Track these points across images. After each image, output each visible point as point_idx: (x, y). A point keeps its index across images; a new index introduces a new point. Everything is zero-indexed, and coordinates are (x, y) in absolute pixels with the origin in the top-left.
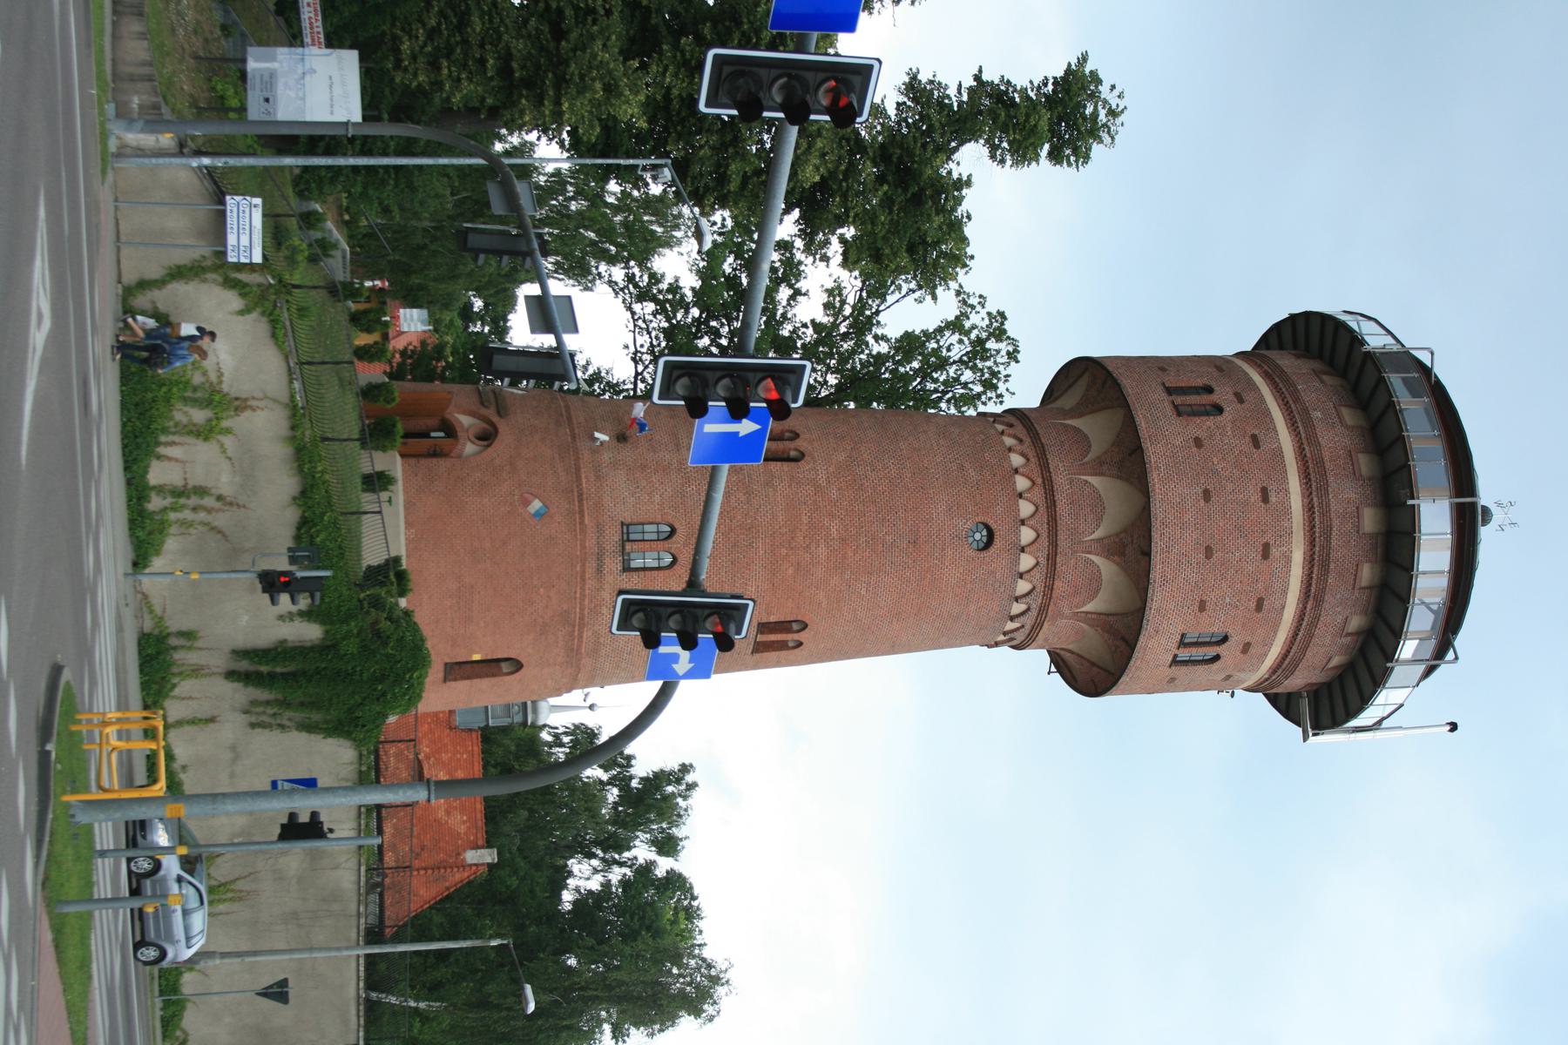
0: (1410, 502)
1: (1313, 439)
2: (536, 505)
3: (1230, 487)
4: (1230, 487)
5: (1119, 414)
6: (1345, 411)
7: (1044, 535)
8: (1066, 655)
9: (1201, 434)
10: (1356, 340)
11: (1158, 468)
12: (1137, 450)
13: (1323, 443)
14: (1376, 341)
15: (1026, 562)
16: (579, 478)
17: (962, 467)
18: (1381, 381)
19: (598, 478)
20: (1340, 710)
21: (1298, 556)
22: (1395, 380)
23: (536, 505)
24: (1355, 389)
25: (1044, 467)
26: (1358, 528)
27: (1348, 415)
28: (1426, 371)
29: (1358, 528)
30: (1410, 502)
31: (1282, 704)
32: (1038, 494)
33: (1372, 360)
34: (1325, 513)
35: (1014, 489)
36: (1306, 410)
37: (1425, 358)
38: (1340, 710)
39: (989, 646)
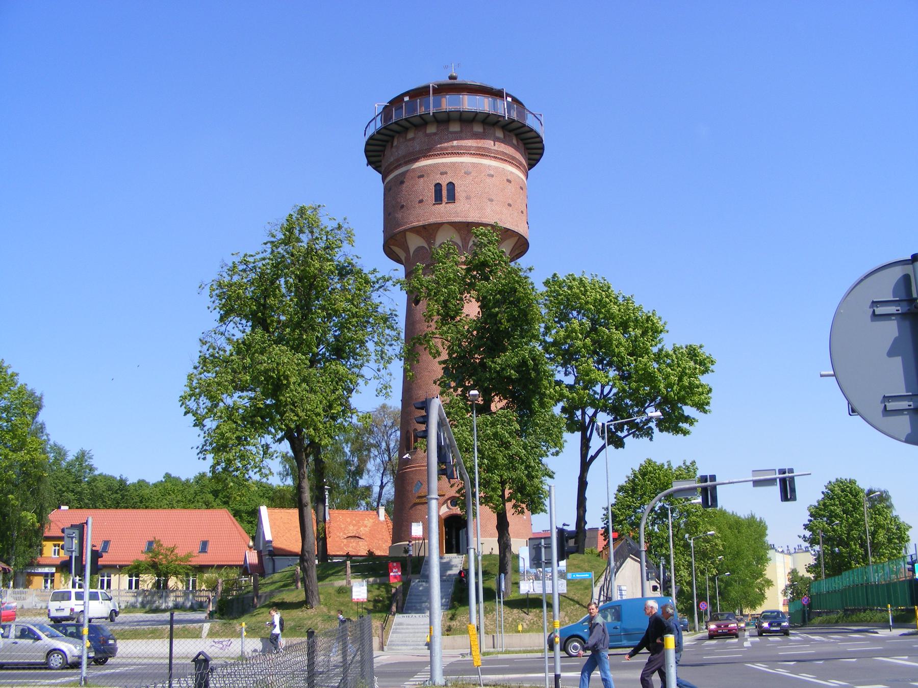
9: (464, 194)
26: (435, 134)
34: (497, 152)
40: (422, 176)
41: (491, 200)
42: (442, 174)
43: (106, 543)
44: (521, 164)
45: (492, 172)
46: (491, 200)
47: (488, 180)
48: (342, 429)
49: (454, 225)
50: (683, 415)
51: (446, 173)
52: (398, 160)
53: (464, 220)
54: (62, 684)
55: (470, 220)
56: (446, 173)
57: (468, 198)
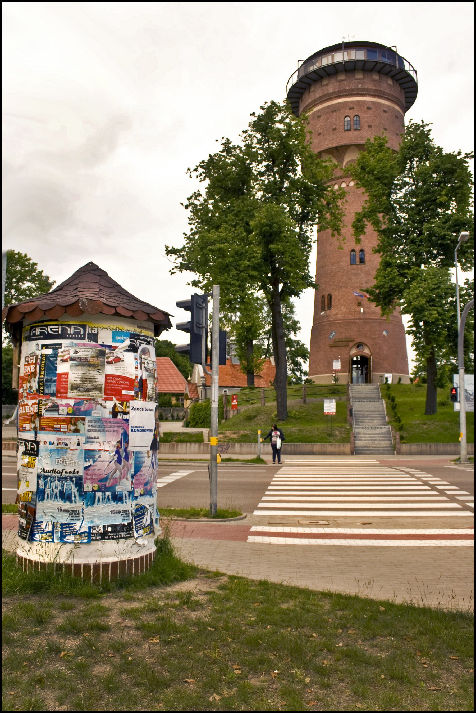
2: (384, 333)
5: (323, 154)
6: (339, 78)
9: (367, 124)
10: (294, 87)
12: (336, 148)
14: (295, 79)
18: (311, 73)
19: (374, 313)
20: (407, 79)
21: (315, 109)
22: (312, 69)
23: (384, 333)
24: (315, 81)
26: (344, 80)
27: (325, 82)
28: (305, 62)
29: (344, 80)
31: (409, 100)
33: (300, 80)
36: (358, 89)
37: (301, 63)
38: (407, 79)
40: (335, 111)
42: (350, 109)
45: (385, 109)
51: (353, 108)
57: (370, 126)
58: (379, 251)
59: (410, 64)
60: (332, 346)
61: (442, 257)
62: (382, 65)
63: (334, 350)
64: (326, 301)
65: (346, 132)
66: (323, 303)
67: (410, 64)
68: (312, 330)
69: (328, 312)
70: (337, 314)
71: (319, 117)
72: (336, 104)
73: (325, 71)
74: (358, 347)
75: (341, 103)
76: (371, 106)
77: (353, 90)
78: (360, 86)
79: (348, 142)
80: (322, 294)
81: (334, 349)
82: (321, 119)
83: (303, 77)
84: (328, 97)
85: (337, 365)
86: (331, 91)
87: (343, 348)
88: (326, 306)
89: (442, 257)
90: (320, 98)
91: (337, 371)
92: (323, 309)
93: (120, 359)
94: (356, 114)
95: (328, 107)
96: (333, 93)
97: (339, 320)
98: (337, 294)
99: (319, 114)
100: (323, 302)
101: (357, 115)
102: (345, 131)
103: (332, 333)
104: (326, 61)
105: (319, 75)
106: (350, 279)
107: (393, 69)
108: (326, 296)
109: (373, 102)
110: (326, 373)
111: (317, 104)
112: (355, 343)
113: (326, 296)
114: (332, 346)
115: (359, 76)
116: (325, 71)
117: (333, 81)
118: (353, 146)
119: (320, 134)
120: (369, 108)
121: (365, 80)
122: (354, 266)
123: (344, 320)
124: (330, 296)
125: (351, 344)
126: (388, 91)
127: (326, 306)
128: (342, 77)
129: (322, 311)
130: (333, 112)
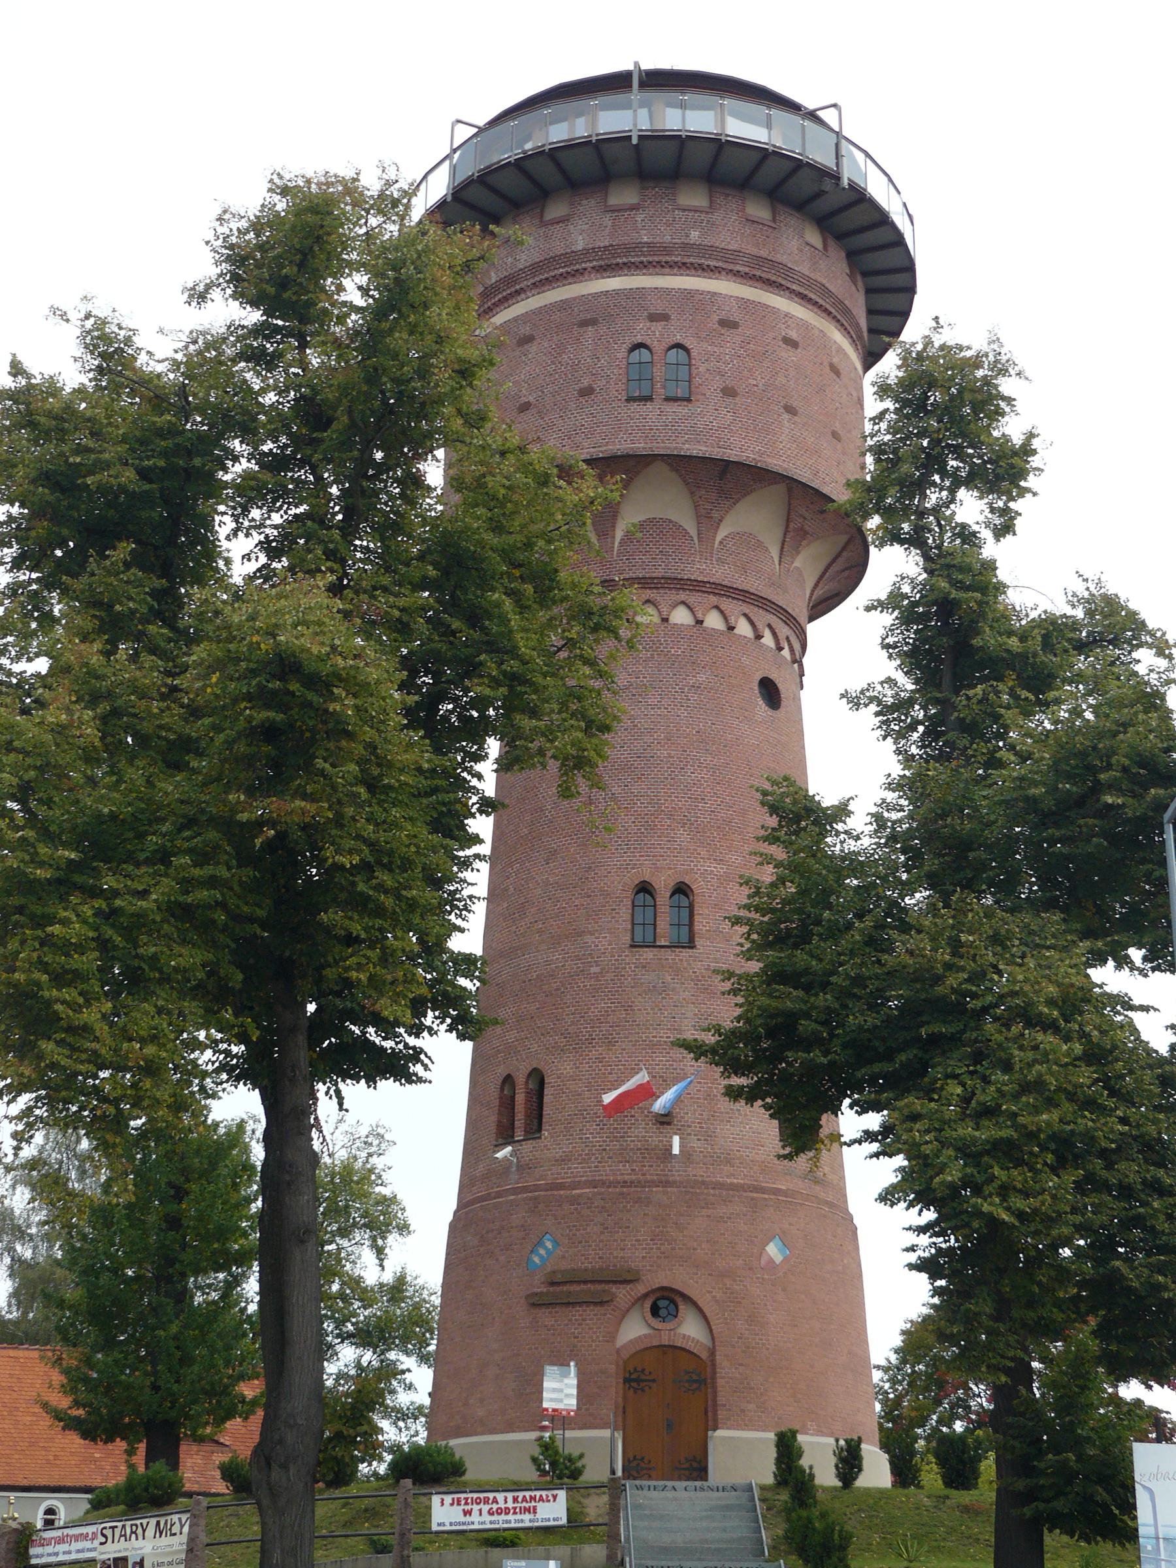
0: (635, 141)
1: (730, 256)
3: (781, 380)
4: (781, 380)
6: (613, 200)
7: (683, 596)
8: (819, 592)
9: (717, 383)
11: (761, 454)
13: (734, 246)
15: (713, 621)
16: (733, 1187)
17: (696, 687)
19: (728, 1162)
25: (697, 586)
26: (634, 208)
27: (556, 209)
29: (634, 208)
30: (635, 141)
31: (884, 322)
32: (665, 598)
34: (808, 282)
35: (722, 633)
36: (686, 246)
39: (802, 674)
40: (593, 322)
41: (791, 410)
42: (653, 318)
43: (1167, 1027)
44: (860, 337)
45: (793, 335)
46: (791, 410)
47: (786, 353)
48: (459, 900)
49: (681, 464)
50: (393, 1287)
51: (665, 317)
52: (509, 280)
53: (717, 453)
54: (430, 1058)
55: (733, 455)
56: (665, 317)
57: (729, 392)
58: (774, 809)
59: (890, 180)
60: (536, 1303)
61: (973, 1387)
62: (788, 166)
63: (550, 1322)
64: (520, 1098)
65: (634, 406)
66: (508, 1109)
67: (890, 180)
68: (453, 1227)
69: (528, 1146)
70: (564, 1160)
71: (528, 339)
72: (597, 296)
73: (558, 165)
74: (655, 1311)
75: (617, 292)
76: (736, 316)
77: (666, 250)
78: (695, 235)
79: (641, 446)
80: (502, 1071)
81: (546, 1317)
82: (533, 348)
83: (468, 183)
84: (568, 268)
85: (560, 1390)
86: (580, 245)
87: (591, 1311)
88: (520, 1122)
89: (973, 1387)
90: (535, 268)
91: (559, 1419)
92: (505, 1135)
93: (12, 362)
94: (678, 338)
95: (564, 306)
96: (587, 252)
97: (574, 1186)
98: (567, 1068)
99: (526, 330)
100: (507, 1104)
101: (678, 346)
102: (629, 400)
103: (540, 1243)
104: (559, 131)
105: (530, 178)
106: (629, 1008)
107: (828, 185)
108: (520, 1079)
109: (745, 303)
110: (510, 1428)
111: (518, 292)
112: (641, 1289)
113: (520, 1079)
114: (536, 1303)
115: (693, 197)
116: (558, 165)
117: (589, 205)
118: (659, 467)
119: (525, 407)
120: (728, 324)
121: (717, 217)
122: (648, 954)
123: (593, 1184)
124: (538, 1079)
125: (623, 1294)
126: (804, 268)
127: (520, 1122)
128: (623, 195)
129: (499, 1146)
130: (584, 323)
